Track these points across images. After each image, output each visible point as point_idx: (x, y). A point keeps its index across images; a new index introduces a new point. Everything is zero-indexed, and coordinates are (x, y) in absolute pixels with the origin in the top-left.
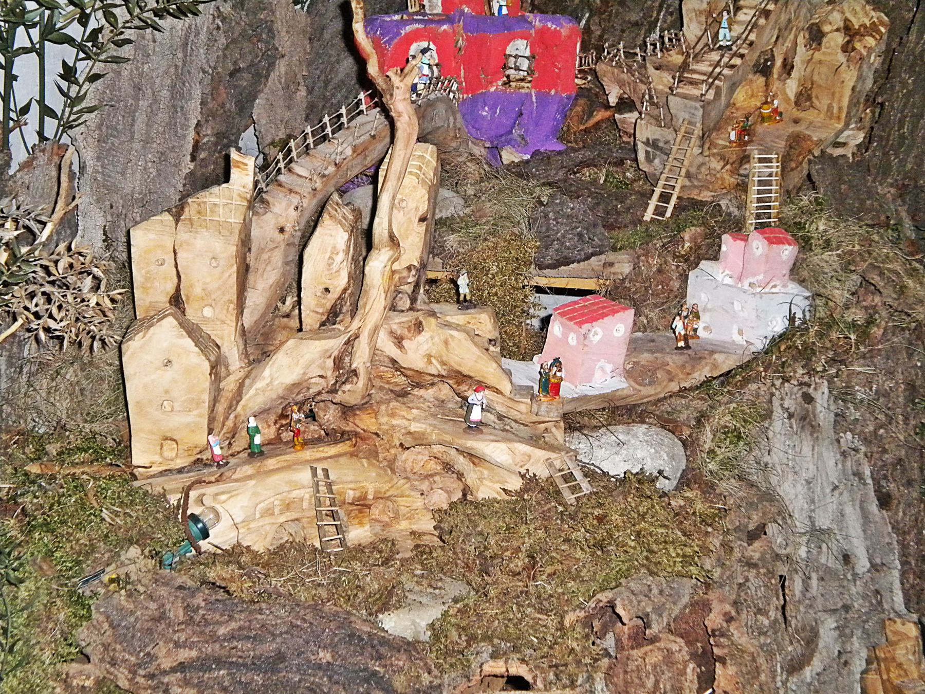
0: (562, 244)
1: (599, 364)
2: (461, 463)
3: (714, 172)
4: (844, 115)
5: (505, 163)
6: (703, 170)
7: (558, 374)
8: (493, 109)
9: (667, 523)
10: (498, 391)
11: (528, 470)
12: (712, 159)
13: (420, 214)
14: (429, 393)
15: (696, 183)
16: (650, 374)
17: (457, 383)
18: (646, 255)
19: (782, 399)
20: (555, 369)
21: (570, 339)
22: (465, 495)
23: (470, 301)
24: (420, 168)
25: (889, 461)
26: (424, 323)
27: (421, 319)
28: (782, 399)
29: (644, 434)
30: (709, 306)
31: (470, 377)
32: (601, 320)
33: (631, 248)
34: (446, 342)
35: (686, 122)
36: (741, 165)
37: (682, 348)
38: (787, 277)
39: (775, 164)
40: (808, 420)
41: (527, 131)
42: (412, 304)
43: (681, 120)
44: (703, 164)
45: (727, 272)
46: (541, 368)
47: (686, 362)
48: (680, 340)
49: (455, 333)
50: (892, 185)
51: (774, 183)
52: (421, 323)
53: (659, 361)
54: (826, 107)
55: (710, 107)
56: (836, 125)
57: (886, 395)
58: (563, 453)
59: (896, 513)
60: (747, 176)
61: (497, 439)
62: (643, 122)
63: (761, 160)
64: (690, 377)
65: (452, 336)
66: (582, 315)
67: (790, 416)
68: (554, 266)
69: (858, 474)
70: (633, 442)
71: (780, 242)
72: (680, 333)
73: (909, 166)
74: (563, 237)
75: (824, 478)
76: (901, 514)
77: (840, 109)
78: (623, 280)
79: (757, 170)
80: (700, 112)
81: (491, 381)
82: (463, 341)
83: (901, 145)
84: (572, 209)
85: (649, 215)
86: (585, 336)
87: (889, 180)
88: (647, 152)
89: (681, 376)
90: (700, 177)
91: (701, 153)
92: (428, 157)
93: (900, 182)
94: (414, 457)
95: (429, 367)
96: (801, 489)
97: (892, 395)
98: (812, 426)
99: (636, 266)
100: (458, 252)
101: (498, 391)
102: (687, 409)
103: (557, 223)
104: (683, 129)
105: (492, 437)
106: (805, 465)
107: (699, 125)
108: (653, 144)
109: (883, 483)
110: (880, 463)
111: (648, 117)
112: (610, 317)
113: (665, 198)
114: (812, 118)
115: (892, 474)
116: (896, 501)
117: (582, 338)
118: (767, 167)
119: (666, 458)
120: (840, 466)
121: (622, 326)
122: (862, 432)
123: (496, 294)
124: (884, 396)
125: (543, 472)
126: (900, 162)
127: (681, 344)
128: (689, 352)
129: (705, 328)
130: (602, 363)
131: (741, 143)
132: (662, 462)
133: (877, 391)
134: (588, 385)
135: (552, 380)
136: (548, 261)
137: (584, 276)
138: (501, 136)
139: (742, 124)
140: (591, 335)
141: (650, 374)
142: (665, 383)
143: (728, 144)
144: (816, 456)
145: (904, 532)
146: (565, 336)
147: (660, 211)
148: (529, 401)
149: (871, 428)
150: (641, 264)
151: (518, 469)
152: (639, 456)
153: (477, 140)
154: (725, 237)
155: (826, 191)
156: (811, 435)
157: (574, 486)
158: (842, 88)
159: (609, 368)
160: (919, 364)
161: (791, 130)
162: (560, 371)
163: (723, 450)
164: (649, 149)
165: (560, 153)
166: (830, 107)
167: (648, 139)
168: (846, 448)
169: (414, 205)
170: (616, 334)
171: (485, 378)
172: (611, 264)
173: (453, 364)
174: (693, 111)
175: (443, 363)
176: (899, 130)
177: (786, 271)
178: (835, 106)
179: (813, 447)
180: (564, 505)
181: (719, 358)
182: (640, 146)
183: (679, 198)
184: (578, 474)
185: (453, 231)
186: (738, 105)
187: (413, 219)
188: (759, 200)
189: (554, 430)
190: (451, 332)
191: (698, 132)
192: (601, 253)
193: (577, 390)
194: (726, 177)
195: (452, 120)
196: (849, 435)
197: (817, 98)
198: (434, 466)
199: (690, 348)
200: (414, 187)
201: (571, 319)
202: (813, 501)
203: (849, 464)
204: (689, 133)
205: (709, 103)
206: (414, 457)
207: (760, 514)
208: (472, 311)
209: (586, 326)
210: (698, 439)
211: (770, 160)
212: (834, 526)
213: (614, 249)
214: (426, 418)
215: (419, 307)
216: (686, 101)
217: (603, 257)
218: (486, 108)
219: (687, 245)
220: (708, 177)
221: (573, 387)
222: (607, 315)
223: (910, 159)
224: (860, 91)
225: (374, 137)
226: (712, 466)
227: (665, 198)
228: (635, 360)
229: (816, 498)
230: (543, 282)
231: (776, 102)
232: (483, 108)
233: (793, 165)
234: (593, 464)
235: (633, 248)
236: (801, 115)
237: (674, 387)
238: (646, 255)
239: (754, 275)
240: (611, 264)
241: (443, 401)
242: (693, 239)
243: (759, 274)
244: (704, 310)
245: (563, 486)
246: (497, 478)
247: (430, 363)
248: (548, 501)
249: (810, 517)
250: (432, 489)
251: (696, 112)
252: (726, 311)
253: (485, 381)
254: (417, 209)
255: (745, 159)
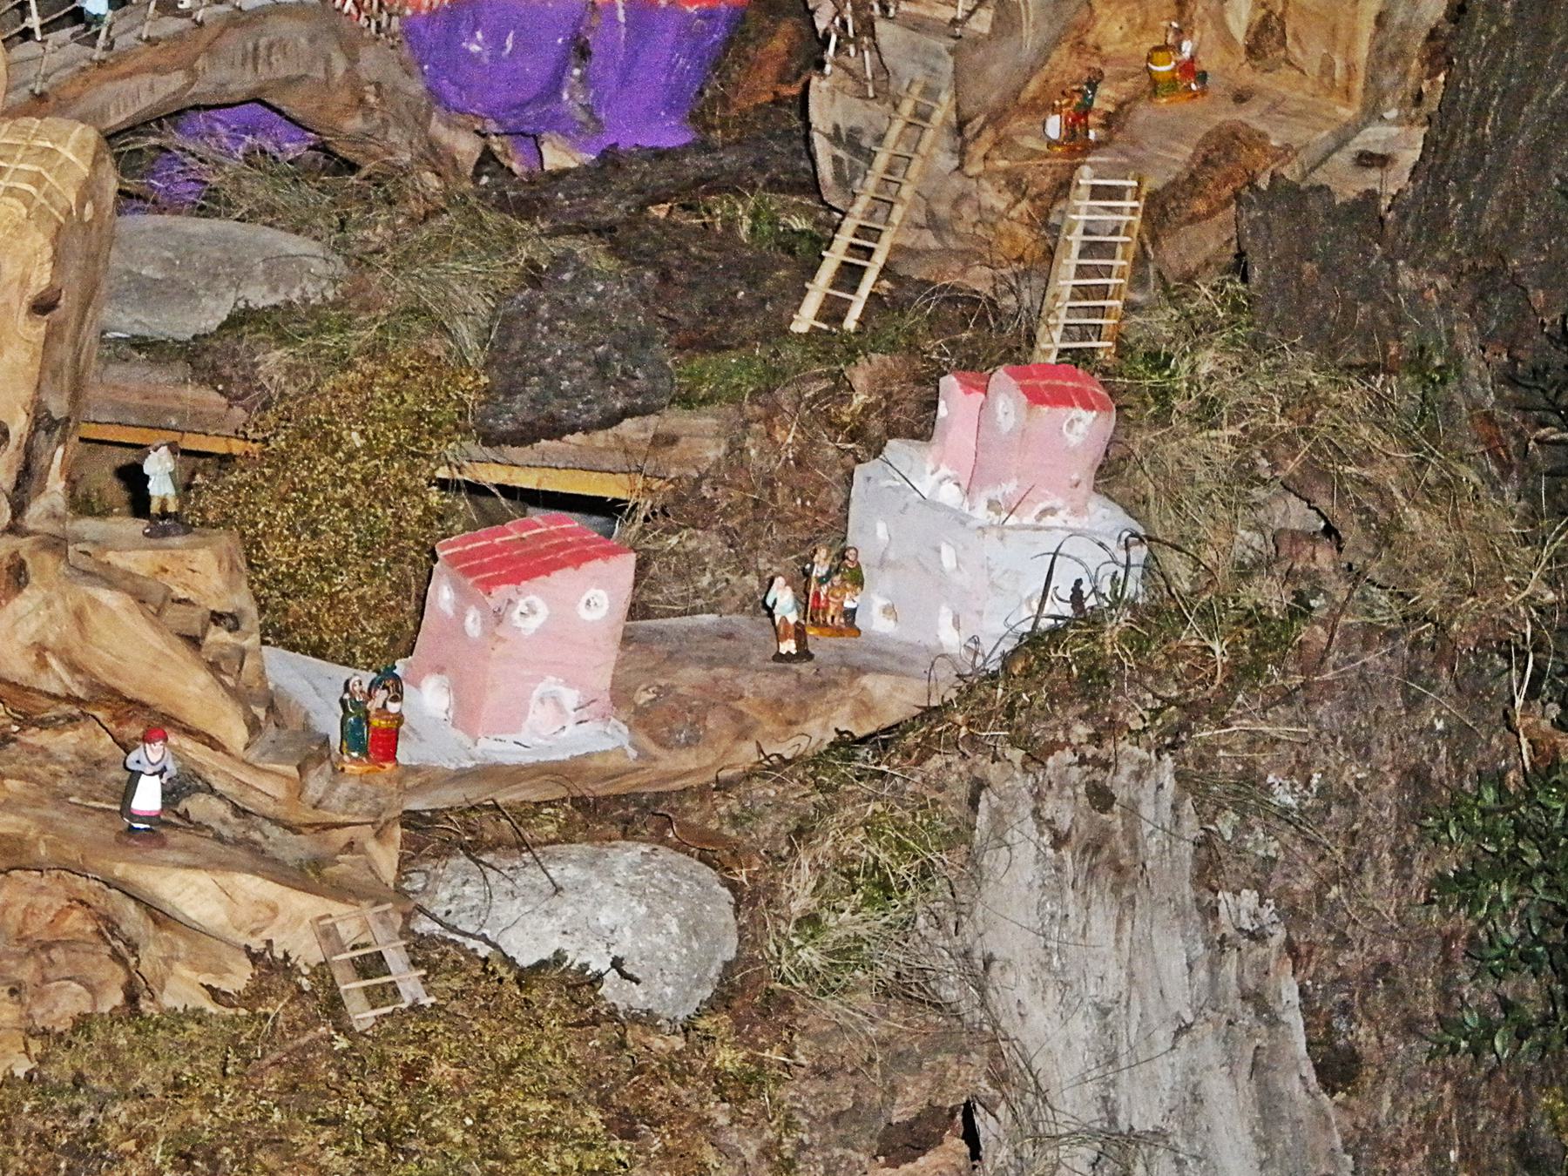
0: (551, 384)
1: (540, 689)
2: (132, 919)
3: (992, 218)
4: (1359, 86)
5: (547, 168)
6: (966, 210)
7: (393, 707)
8: (496, 39)
9: (568, 1089)
10: (213, 743)
11: (269, 943)
12: (985, 184)
13: (33, 292)
14: (65, 742)
15: (952, 242)
16: (690, 718)
17: (114, 717)
18: (768, 419)
19: (1038, 797)
20: (381, 695)
21: (469, 620)
22: (132, 998)
23: (176, 516)
24: (38, 180)
25: (1353, 969)
26: (29, 566)
27: (23, 555)
28: (1038, 797)
29: (632, 867)
30: (892, 556)
31: (144, 706)
32: (542, 578)
33: (730, 401)
34: (79, 616)
35: (916, 90)
36: (1056, 199)
37: (788, 657)
38: (1085, 488)
39: (1128, 203)
40: (1106, 853)
41: (598, 97)
42: (14, 517)
43: (906, 84)
44: (963, 197)
45: (944, 471)
46: (346, 689)
47: (786, 692)
48: (786, 637)
49: (105, 596)
50: (1443, 269)
51: (1120, 250)
52: (22, 564)
53: (724, 687)
54: (1317, 64)
55: (979, 55)
56: (1342, 110)
57: (1349, 799)
58: (364, 904)
59: (1376, 1102)
60: (1058, 228)
61: (199, 861)
62: (825, 84)
63: (1096, 192)
64: (796, 729)
65: (95, 602)
66: (500, 563)
67: (1059, 841)
68: (525, 436)
69: (1257, 1000)
70: (597, 885)
71: (1061, 398)
72: (784, 619)
73: (1487, 223)
74: (559, 365)
75: (1152, 1000)
76: (1387, 1103)
77: (1350, 69)
78: (697, 483)
79: (1081, 211)
80: (947, 65)
81: (196, 716)
82: (125, 617)
83: (1474, 165)
84: (598, 296)
85: (805, 319)
86: (499, 617)
87: (1441, 256)
88: (836, 160)
89: (769, 728)
90: (961, 228)
91: (959, 168)
92: (67, 152)
93: (1466, 263)
94: (29, 899)
95: (43, 677)
96: (1082, 1027)
97: (1363, 800)
98: (1119, 870)
99: (736, 447)
100: (283, 395)
101: (213, 743)
102: (779, 810)
103: (552, 330)
104: (907, 107)
105: (181, 857)
106: (1097, 967)
107: (945, 98)
108: (847, 139)
109: (1340, 1024)
110: (1330, 974)
111: (840, 72)
112: (570, 571)
113: (849, 275)
114: (1283, 90)
115: (1363, 999)
116: (1373, 1072)
117: (492, 620)
118: (1109, 209)
119: (675, 929)
120: (1202, 975)
121: (601, 593)
122: (1285, 891)
123: (346, 503)
124: (1341, 802)
125: (305, 950)
126: (1468, 211)
127: (789, 646)
128: (805, 668)
129: (889, 611)
130: (550, 684)
131: (1076, 145)
132: (660, 940)
133: (1321, 789)
134: (510, 738)
135: (375, 722)
136: (505, 425)
137: (607, 466)
138: (523, 105)
139: (1078, 99)
140: (516, 615)
141: (690, 718)
142: (726, 743)
143: (1044, 148)
144: (1126, 944)
145: (1395, 1153)
146: (461, 614)
147: (833, 311)
148: (292, 770)
149: (1307, 882)
150: (749, 441)
151: (242, 939)
152: (603, 921)
153: (456, 114)
154: (949, 383)
155: (1265, 277)
156: (1116, 889)
157: (383, 986)
158: (1355, 16)
159: (571, 698)
160: (1440, 725)
161: (1220, 118)
162: (395, 699)
163: (845, 916)
164: (840, 153)
165: (659, 155)
166: (1327, 68)
167: (837, 128)
168: (1229, 931)
169: (18, 272)
170: (586, 615)
171: (180, 709)
172: (671, 440)
173: (99, 670)
174: (931, 61)
175: (74, 668)
176: (1475, 125)
177: (1082, 470)
178: (1339, 65)
179: (1120, 922)
180: (347, 1031)
181: (876, 685)
182: (821, 145)
183: (885, 271)
184: (396, 958)
185: (283, 339)
186: (1107, 49)
187: (15, 306)
188: (1083, 292)
189: (372, 845)
190: (91, 591)
191: (943, 110)
192: (645, 411)
193: (477, 751)
194: (1022, 232)
195: (340, 65)
196: (1249, 898)
197: (1296, 38)
198: (79, 925)
199: (810, 657)
200: (17, 227)
201: (469, 572)
202: (1112, 1059)
203: (1230, 968)
204: (923, 116)
205: (976, 42)
206: (29, 899)
207: (926, 1083)
208: (177, 541)
209: (502, 592)
210: (774, 888)
211: (1118, 193)
212: (1173, 1126)
213: (687, 401)
214: (37, 802)
215: (30, 526)
216: (915, 36)
217: (652, 420)
218: (479, 35)
219: (859, 399)
220: (979, 231)
221: (468, 742)
222: (561, 565)
223: (1493, 203)
224: (1403, 27)
225: (42, 97)
226: (811, 956)
227: (849, 275)
228: (663, 682)
229: (1124, 1048)
230: (491, 475)
231: (1187, 47)
232: (473, 35)
233: (1200, 206)
234: (484, 938)
235: (734, 399)
236: (1261, 80)
237: (746, 754)
238: (768, 419)
239: (997, 481)
240: (671, 440)
241: (97, 764)
242: (880, 382)
243: (1008, 480)
244: (883, 563)
245: (351, 988)
246: (206, 961)
247: (43, 664)
248: (311, 1022)
249: (1105, 1099)
250: (45, 980)
251: (940, 65)
252: (926, 570)
253: (180, 717)
254: (24, 282)
255: (1063, 187)
